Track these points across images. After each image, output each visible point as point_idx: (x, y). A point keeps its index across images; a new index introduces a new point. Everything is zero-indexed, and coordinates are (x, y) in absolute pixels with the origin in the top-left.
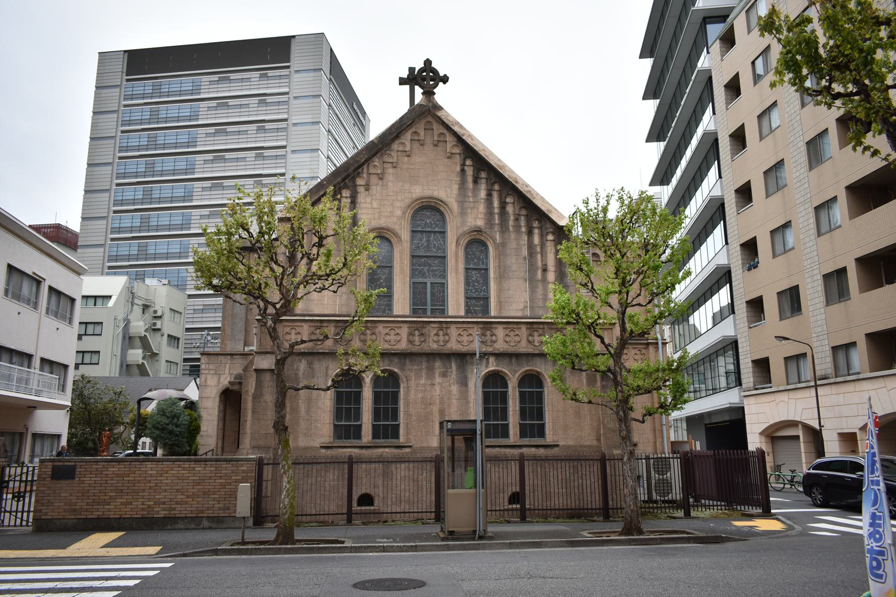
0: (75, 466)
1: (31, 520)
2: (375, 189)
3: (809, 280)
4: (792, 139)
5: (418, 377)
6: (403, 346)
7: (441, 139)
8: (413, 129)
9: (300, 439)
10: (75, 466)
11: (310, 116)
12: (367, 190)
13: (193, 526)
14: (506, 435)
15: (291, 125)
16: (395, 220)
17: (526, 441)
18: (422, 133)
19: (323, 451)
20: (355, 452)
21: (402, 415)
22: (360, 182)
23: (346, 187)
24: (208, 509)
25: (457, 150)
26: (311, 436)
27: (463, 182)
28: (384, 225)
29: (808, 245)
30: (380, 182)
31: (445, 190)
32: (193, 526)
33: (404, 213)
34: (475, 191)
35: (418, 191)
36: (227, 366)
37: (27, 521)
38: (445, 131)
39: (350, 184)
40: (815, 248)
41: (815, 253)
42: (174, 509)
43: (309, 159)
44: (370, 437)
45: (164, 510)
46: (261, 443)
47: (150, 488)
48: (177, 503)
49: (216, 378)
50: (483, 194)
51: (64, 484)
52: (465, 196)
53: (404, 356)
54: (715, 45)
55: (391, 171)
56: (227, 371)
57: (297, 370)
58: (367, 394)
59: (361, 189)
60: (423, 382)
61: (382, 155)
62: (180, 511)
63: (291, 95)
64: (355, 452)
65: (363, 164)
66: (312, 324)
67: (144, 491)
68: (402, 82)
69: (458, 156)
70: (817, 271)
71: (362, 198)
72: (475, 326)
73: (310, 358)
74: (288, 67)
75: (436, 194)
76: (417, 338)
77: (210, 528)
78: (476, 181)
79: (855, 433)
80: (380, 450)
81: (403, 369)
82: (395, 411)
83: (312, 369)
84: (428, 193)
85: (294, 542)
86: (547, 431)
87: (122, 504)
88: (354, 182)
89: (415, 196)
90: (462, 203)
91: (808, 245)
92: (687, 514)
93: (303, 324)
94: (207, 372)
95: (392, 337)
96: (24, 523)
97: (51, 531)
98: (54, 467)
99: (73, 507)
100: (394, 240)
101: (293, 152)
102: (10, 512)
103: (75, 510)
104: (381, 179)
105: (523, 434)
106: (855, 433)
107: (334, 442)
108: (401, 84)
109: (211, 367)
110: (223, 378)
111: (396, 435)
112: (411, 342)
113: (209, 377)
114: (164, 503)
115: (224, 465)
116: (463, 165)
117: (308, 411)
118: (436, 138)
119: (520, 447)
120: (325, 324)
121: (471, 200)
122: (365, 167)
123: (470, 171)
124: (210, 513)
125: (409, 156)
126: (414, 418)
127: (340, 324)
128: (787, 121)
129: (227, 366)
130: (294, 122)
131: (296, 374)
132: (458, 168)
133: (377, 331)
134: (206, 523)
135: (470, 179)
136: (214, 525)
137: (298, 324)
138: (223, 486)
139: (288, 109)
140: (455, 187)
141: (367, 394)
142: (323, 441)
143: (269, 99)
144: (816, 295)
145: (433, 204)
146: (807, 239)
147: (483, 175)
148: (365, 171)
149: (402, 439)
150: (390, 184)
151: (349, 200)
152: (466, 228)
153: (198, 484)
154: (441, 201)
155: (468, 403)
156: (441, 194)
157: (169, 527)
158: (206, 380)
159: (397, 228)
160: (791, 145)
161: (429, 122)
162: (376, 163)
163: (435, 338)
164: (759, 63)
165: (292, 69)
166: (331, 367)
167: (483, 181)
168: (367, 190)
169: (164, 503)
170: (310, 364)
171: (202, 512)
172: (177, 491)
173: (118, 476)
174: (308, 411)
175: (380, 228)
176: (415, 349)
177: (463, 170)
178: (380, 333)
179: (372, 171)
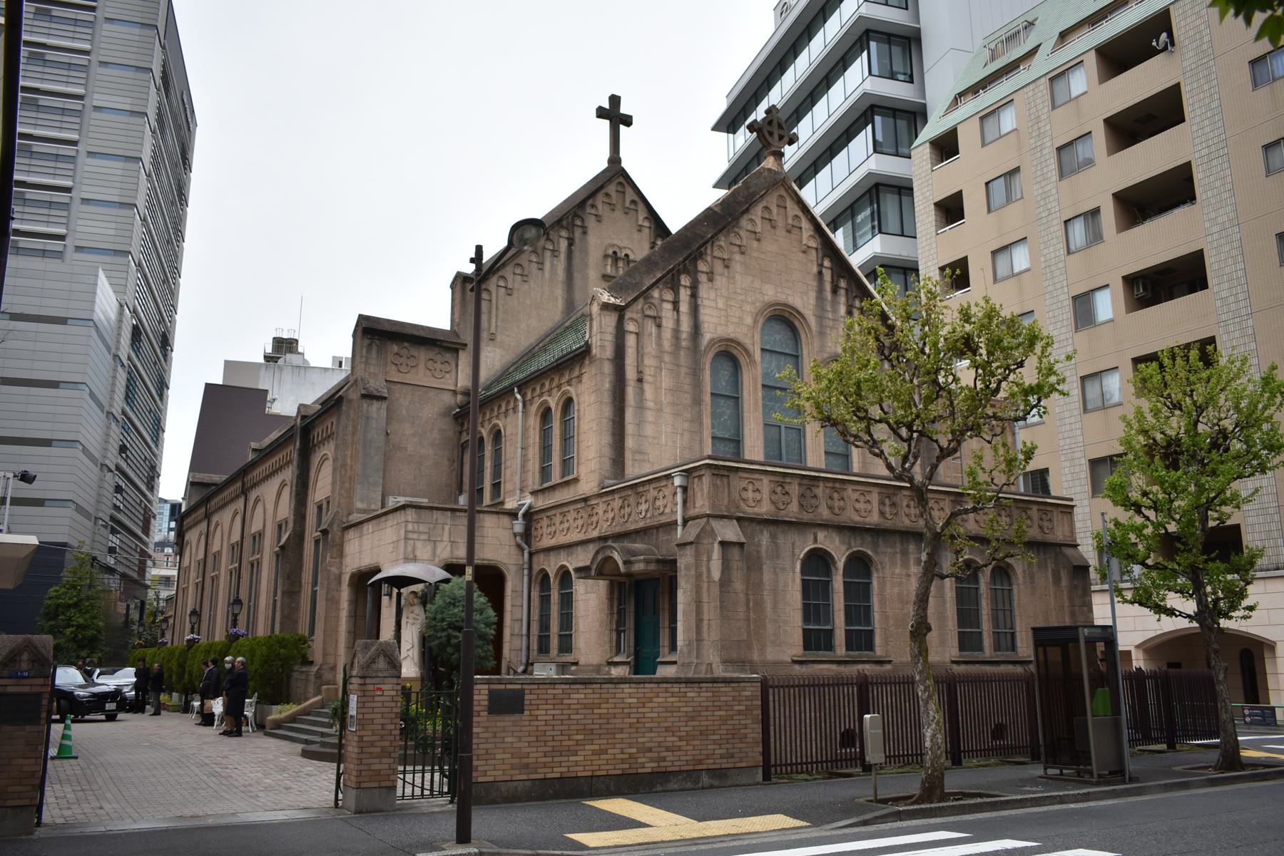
0: (523, 690)
1: (400, 783)
2: (720, 281)
3: (1067, 464)
4: (1050, 288)
5: (893, 564)
6: (874, 519)
7: (796, 224)
8: (764, 203)
9: (769, 649)
10: (523, 690)
11: (129, 101)
12: (711, 280)
13: (689, 785)
14: (830, 647)
15: (77, 202)
16: (745, 330)
17: (813, 655)
18: (774, 210)
19: (797, 667)
20: (868, 669)
21: (876, 616)
22: (702, 266)
23: (686, 271)
24: (708, 757)
25: (813, 244)
26: (780, 645)
27: (820, 290)
28: (732, 336)
29: (1067, 421)
30: (726, 271)
31: (803, 300)
32: (689, 785)
33: (755, 322)
34: (835, 304)
35: (771, 293)
36: (447, 527)
37: (432, 790)
38: (800, 214)
39: (691, 268)
40: (1078, 425)
41: (1079, 432)
42: (664, 759)
43: (120, 172)
44: (801, 648)
45: (651, 760)
46: (734, 655)
47: (631, 725)
48: (668, 749)
49: (429, 548)
50: (842, 310)
51: (507, 721)
52: (823, 310)
53: (877, 533)
54: (921, 148)
55: (738, 257)
56: (446, 537)
57: (759, 545)
58: (838, 583)
59: (703, 278)
60: (897, 571)
61: (729, 232)
62: (673, 761)
63: (93, 57)
64: (868, 669)
65: (707, 242)
66: (773, 478)
67: (622, 730)
68: (615, 100)
69: (814, 252)
70: (1078, 455)
71: (704, 291)
72: (946, 497)
73: (772, 528)
74: (93, 9)
75: (791, 301)
76: (887, 509)
77: (711, 787)
78: (835, 291)
79: (1129, 652)
80: (860, 667)
81: (876, 553)
82: (868, 609)
83: (776, 545)
84: (782, 298)
85: (944, 797)
86: (878, 640)
87: (594, 753)
88: (696, 267)
89: (767, 299)
90: (820, 318)
91: (1067, 421)
92: (1171, 746)
93: (762, 477)
94: (415, 536)
95: (861, 506)
96: (427, 793)
97: (493, 802)
98: (491, 691)
99: (525, 761)
100: (743, 360)
101: (91, 154)
102: (817, 762)
103: (527, 766)
104: (727, 267)
105: (849, 647)
106: (1129, 652)
107: (804, 655)
108: (599, 116)
109: (422, 528)
110: (440, 547)
111: (870, 647)
112: (882, 513)
113: (419, 544)
114: (650, 750)
115: (724, 688)
116: (821, 265)
117: (775, 607)
118: (790, 221)
119: (998, 663)
120: (788, 480)
121: (830, 316)
122: (709, 246)
123: (827, 275)
124: (709, 763)
125: (758, 240)
126: (891, 622)
127: (806, 482)
128: (1043, 266)
129: (447, 527)
130: (95, 103)
131: (758, 552)
132: (815, 269)
133: (845, 494)
134: (705, 779)
135: (828, 287)
136: (716, 783)
137: (756, 476)
138: (723, 720)
139: (87, 79)
140: (813, 295)
141: (838, 583)
142: (794, 652)
143: (50, 55)
144: (1077, 483)
145: (786, 315)
146: (1067, 414)
147: (843, 284)
148: (709, 251)
149: (879, 651)
150: (738, 277)
151: (689, 292)
152: (826, 355)
153: (693, 719)
154: (798, 312)
155: (944, 602)
156: (797, 302)
157: (660, 788)
158: (414, 550)
159: (747, 341)
160: (1047, 296)
161: (781, 196)
162: (722, 243)
163: (907, 510)
164: (999, 186)
165: (98, 13)
166: (797, 543)
167: (842, 292)
168: (711, 280)
169: (650, 750)
170: (773, 537)
171: (700, 762)
172: (667, 729)
173: (586, 706)
174: (775, 607)
175: (729, 340)
176: (888, 524)
177: (820, 273)
178: (849, 498)
179: (716, 253)
